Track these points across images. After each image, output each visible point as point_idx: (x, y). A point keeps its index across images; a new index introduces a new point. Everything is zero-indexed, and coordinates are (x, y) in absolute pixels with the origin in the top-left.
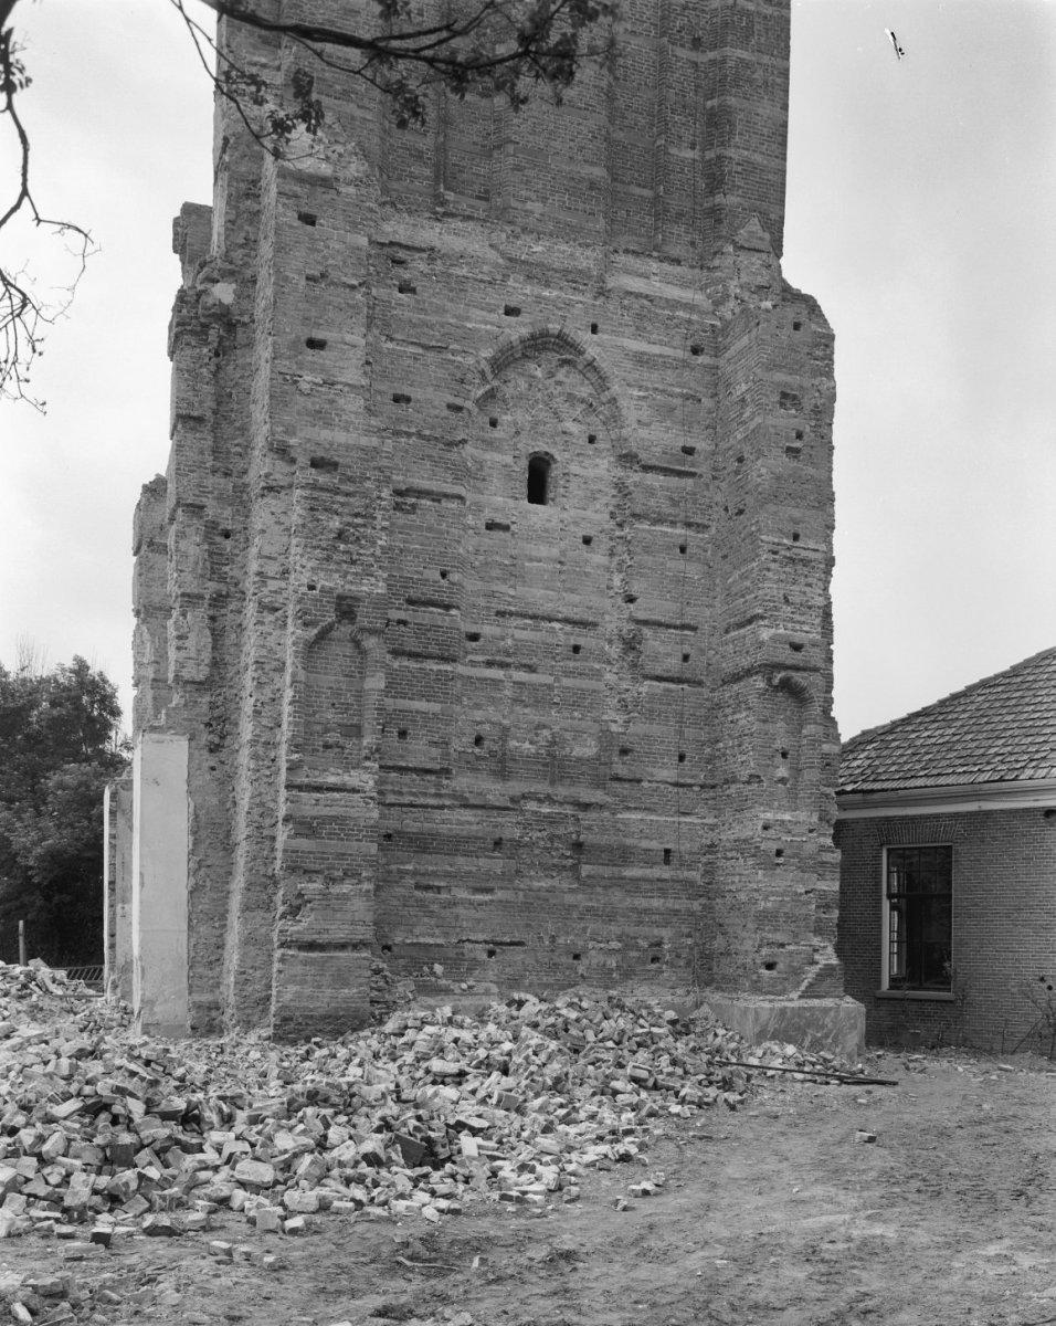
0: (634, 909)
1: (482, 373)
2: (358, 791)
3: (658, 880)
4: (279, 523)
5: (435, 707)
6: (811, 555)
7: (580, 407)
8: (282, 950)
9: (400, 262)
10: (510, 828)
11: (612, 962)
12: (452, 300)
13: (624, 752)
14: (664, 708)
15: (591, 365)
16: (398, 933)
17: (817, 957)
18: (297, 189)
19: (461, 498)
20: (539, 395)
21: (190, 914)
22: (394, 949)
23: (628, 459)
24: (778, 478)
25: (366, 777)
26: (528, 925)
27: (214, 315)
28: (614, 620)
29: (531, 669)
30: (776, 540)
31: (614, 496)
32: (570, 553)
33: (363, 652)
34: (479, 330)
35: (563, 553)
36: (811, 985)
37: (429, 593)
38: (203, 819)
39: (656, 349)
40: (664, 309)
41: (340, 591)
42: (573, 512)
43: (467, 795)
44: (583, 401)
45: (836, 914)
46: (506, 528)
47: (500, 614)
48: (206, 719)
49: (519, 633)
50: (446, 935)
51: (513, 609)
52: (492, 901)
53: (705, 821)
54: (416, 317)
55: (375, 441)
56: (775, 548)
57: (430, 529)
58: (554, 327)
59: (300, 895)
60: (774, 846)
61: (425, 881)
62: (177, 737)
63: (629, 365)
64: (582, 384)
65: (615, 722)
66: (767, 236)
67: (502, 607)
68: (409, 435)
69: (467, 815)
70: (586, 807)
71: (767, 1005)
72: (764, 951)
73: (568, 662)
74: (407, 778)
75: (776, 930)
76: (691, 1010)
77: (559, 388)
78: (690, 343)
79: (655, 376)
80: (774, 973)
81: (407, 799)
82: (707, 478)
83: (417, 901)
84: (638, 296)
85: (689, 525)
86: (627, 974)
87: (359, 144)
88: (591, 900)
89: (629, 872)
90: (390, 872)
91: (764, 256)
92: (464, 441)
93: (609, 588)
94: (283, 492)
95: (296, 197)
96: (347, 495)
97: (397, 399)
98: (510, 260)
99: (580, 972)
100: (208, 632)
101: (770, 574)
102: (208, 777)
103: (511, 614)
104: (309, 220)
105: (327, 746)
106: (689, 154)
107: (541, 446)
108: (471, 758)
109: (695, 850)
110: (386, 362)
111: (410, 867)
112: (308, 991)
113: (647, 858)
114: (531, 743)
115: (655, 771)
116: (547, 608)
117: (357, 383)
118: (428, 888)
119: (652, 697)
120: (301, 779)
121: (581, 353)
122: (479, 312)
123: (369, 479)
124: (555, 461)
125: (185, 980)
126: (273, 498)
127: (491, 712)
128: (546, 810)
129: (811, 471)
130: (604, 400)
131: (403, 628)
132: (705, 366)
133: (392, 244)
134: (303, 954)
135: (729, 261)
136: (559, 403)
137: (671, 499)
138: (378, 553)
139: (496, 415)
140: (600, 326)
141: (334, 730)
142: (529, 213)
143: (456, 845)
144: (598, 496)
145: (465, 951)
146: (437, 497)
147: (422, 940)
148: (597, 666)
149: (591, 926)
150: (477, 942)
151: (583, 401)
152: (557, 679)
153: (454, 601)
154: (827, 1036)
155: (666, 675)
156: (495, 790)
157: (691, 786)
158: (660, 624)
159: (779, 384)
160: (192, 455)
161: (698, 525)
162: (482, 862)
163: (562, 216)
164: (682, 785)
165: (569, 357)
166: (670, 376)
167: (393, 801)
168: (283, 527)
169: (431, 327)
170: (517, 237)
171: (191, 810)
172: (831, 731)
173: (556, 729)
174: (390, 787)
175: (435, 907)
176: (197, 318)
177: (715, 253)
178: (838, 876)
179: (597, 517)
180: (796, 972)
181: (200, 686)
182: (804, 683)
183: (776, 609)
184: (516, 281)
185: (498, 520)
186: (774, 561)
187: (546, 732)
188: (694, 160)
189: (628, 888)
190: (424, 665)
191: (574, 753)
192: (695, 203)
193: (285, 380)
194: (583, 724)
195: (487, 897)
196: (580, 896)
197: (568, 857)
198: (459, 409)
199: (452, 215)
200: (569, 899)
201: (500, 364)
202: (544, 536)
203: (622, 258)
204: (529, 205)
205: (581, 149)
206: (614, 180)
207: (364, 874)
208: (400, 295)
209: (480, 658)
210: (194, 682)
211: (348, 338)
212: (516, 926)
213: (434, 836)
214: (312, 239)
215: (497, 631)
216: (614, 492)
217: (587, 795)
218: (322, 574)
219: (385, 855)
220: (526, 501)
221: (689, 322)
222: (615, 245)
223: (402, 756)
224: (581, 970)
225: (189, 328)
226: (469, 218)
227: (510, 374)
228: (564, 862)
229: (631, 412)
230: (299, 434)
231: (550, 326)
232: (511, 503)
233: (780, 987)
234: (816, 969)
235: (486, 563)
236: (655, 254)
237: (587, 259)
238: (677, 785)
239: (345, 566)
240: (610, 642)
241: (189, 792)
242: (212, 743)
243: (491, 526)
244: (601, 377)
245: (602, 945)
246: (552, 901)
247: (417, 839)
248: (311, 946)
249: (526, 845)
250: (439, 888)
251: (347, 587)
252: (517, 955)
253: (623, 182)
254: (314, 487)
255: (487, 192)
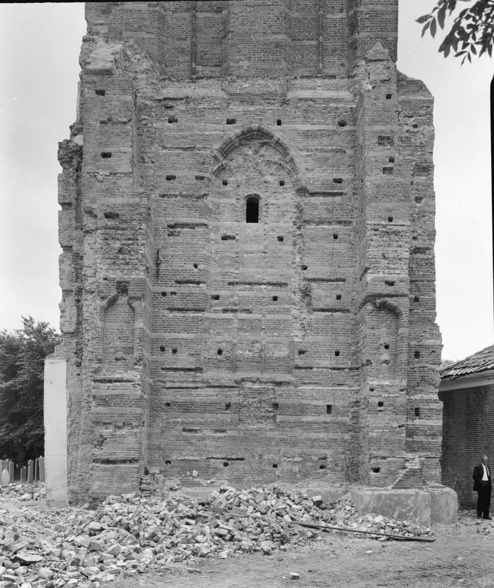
0: (308, 439)
1: (215, 157)
2: (131, 381)
3: (323, 423)
4: (92, 249)
5: (191, 336)
6: (400, 229)
7: (274, 167)
8: (93, 464)
9: (171, 107)
10: (234, 397)
11: (296, 469)
12: (197, 122)
13: (301, 352)
14: (325, 326)
15: (278, 143)
16: (174, 454)
17: (407, 464)
18: (94, 78)
19: (205, 225)
20: (250, 164)
21: (68, 447)
22: (172, 462)
23: (302, 191)
24: (377, 187)
25: (136, 374)
26: (246, 449)
27: (73, 151)
28: (296, 282)
29: (249, 311)
30: (376, 223)
31: (294, 213)
32: (269, 247)
33: (133, 309)
34: (212, 135)
35: (266, 247)
36: (400, 481)
37: (188, 277)
38: (74, 400)
39: (316, 127)
40: (322, 104)
41: (118, 279)
42: (271, 224)
43: (210, 381)
44: (276, 163)
45: (440, 439)
46: (233, 238)
47: (230, 284)
48: (75, 351)
49: (242, 292)
50: (200, 455)
51: (237, 280)
52: (225, 437)
53: (352, 388)
54: (177, 134)
55: (137, 200)
56: (377, 227)
57: (187, 243)
58: (255, 126)
59: (102, 436)
60: (377, 400)
61: (188, 427)
62: (61, 360)
63: (300, 139)
64: (275, 154)
65: (297, 336)
66: (387, 51)
67: (231, 280)
68: (176, 196)
69: (211, 391)
70: (279, 384)
71: (370, 493)
72: (373, 461)
73: (270, 306)
74: (177, 374)
75: (379, 449)
76: (341, 495)
77: (262, 158)
78: (337, 120)
79: (316, 142)
80: (378, 474)
81: (177, 385)
82: (350, 194)
83: (183, 437)
84: (306, 100)
85: (340, 222)
86: (305, 475)
87: (147, 52)
88: (283, 434)
89: (305, 419)
90: (169, 423)
91: (385, 63)
92: (205, 195)
93: (293, 263)
94: (94, 233)
95: (94, 82)
96: (123, 229)
97: (169, 178)
98: (231, 95)
99: (277, 474)
100: (75, 308)
101: (372, 243)
102: (76, 379)
103: (237, 283)
104: (101, 93)
105: (117, 359)
106: (339, 16)
107: (252, 191)
108: (215, 361)
109: (347, 405)
110: (162, 160)
111: (179, 420)
112: (106, 484)
113: (316, 411)
114: (249, 351)
115: (321, 362)
116: (257, 278)
117: (127, 171)
118: (191, 431)
119: (317, 321)
120: (100, 377)
121: (272, 137)
122: (211, 125)
123: (135, 220)
124: (260, 197)
125: (66, 479)
126: (89, 237)
127: (226, 336)
128: (256, 386)
129: (399, 179)
130: (287, 161)
131: (174, 296)
132: (347, 132)
133: (165, 99)
134: (103, 465)
135: (363, 69)
136: (263, 167)
137: (328, 209)
138: (140, 257)
139: (225, 179)
140: (282, 121)
141: (120, 351)
142: (240, 67)
143: (205, 407)
144: (285, 214)
145: (211, 463)
146: (192, 226)
147: (187, 458)
148: (287, 306)
149: (283, 449)
150: (218, 459)
151: (276, 163)
152: (264, 315)
153: (201, 279)
154: (409, 511)
155: (326, 308)
156: (226, 376)
157: (343, 369)
158: (323, 280)
159: (377, 132)
160: (66, 222)
161: (345, 222)
162: (219, 416)
163: (260, 65)
164: (339, 369)
165: (266, 140)
166: (325, 141)
167: (170, 386)
168: (94, 251)
169: (186, 138)
170: (234, 82)
171: (68, 395)
172: (435, 332)
173: (264, 342)
174: (168, 379)
175: (193, 441)
176: (67, 154)
177: (354, 67)
178: (441, 417)
179: (286, 225)
180: (393, 473)
181: (72, 334)
182: (395, 304)
183: (377, 262)
184: (234, 105)
185: (228, 234)
186: (376, 235)
187: (258, 345)
188: (342, 18)
189: (305, 427)
190: (186, 315)
191: (275, 355)
192: (343, 42)
193: (90, 176)
194: (280, 339)
195: (223, 435)
196: (276, 433)
197: (271, 412)
198: (202, 178)
199: (201, 78)
200: (270, 434)
201: (227, 150)
202: (255, 239)
203: (299, 82)
204: (241, 63)
205: (270, 27)
206: (293, 40)
207: (134, 424)
208: (170, 124)
209: (220, 308)
210: (69, 333)
211: (122, 149)
212: (239, 449)
213: (192, 403)
214: (103, 102)
215: (228, 293)
216: (295, 210)
217: (280, 377)
218: (111, 272)
219: (166, 415)
220: (245, 222)
221: (337, 108)
222: (295, 75)
223: (174, 363)
224: (277, 473)
225: (64, 160)
226: (211, 77)
227: (234, 155)
228: (268, 414)
229: (301, 165)
230: (98, 202)
231: (253, 125)
232: (236, 224)
233: (382, 482)
234: (404, 472)
235: (222, 258)
236: (319, 75)
237: (274, 86)
238: (334, 369)
239: (122, 266)
240: (294, 293)
241: (67, 387)
242: (77, 362)
243: (225, 238)
244: (284, 149)
245: (290, 459)
246: (260, 436)
247: (184, 405)
248: (108, 462)
249: (245, 406)
250: (196, 430)
251: (124, 276)
252: (240, 465)
253: (299, 40)
254: (106, 227)
255: (219, 62)
